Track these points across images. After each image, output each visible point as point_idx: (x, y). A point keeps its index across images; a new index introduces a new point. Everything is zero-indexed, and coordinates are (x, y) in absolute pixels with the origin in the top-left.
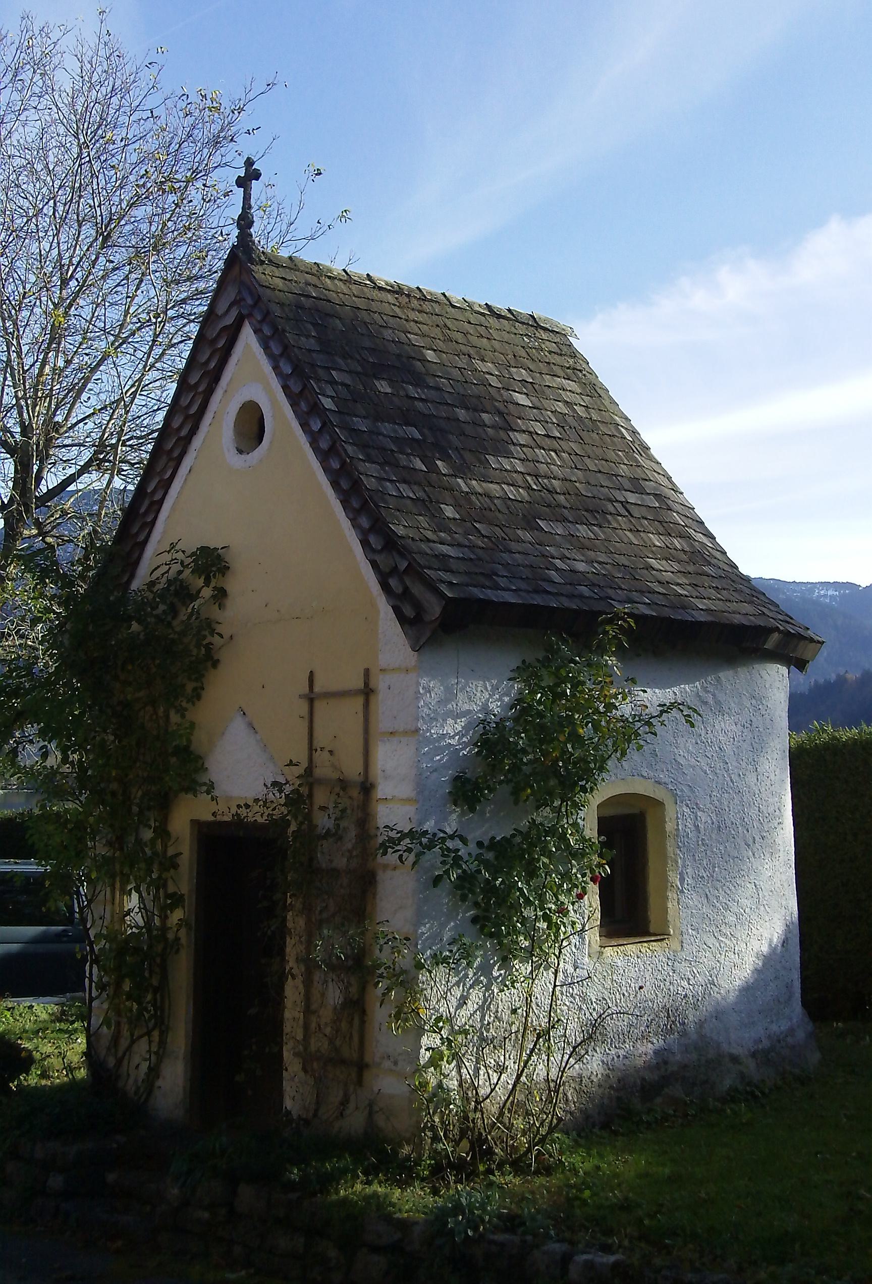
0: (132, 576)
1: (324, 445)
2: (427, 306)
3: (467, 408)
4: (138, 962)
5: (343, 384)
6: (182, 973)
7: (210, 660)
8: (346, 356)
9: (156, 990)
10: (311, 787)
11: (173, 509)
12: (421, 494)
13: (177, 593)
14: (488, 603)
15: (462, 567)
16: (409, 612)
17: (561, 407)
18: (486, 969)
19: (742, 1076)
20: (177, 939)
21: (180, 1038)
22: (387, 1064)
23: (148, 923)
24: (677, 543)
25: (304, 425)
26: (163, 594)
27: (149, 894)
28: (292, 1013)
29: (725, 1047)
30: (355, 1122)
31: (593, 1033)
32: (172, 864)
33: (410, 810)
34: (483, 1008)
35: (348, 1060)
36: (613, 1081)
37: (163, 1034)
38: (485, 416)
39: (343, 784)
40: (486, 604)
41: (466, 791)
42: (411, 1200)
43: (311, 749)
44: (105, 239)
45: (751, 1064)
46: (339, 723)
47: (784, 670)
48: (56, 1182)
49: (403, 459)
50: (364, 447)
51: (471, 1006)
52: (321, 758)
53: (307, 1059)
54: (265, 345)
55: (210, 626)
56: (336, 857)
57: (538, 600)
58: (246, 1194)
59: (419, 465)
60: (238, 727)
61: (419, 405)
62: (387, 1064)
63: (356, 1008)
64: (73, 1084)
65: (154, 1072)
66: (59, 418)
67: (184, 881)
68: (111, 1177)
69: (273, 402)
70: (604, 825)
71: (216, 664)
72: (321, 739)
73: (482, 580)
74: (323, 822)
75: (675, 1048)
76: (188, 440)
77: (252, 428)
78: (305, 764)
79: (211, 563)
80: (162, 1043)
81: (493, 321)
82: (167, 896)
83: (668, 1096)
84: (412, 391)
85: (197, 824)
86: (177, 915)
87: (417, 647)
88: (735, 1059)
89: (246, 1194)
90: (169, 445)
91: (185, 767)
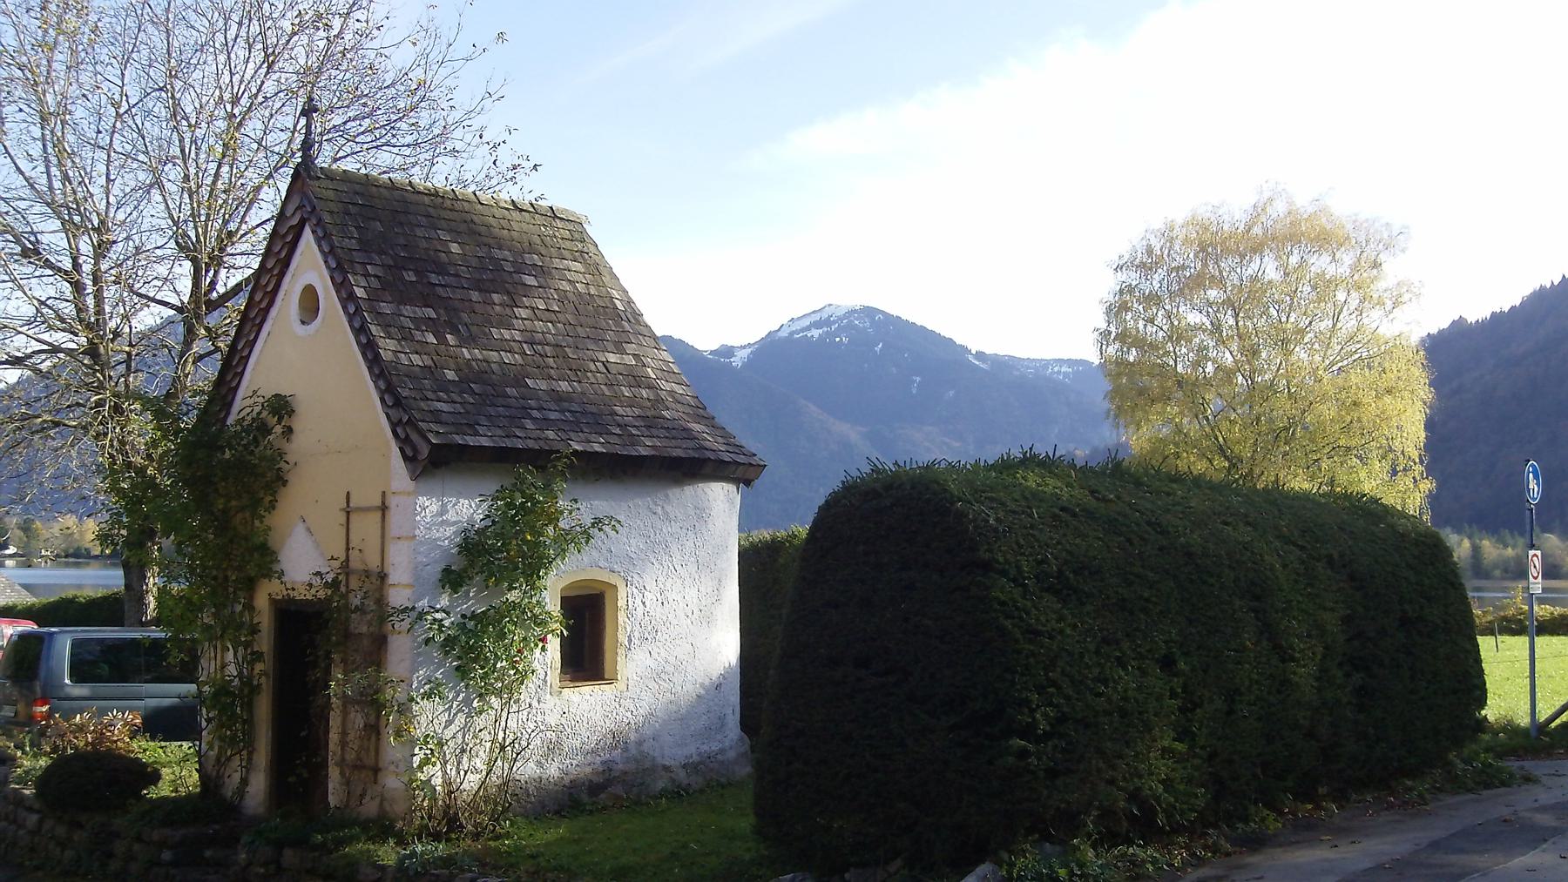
0: (228, 414)
1: (357, 325)
2: (458, 206)
3: (480, 291)
4: (230, 702)
5: (375, 276)
6: (263, 708)
7: (281, 480)
8: (381, 252)
9: (245, 722)
10: (347, 574)
11: (257, 363)
12: (429, 363)
13: (258, 428)
14: (466, 446)
15: (451, 419)
16: (409, 453)
17: (565, 286)
18: (467, 702)
19: (673, 780)
20: (259, 685)
21: (262, 757)
22: (392, 768)
23: (240, 674)
24: (644, 393)
25: (345, 308)
26: (247, 430)
27: (1544, 809)
28: (334, 737)
29: (659, 761)
30: (370, 808)
31: (553, 749)
32: (254, 630)
33: (407, 592)
34: (465, 729)
35: (369, 768)
36: (567, 780)
37: (250, 754)
38: (495, 296)
39: (367, 573)
40: (465, 448)
41: (452, 579)
42: (388, 854)
43: (348, 549)
44: (269, 67)
45: (682, 774)
46: (365, 528)
47: (731, 487)
48: (167, 855)
49: (418, 335)
50: (386, 326)
51: (453, 728)
52: (354, 554)
53: (342, 763)
54: (318, 241)
55: (281, 454)
56: (360, 626)
57: (508, 443)
58: (289, 856)
59: (431, 339)
60: (300, 530)
61: (440, 291)
62: (392, 768)
63: (374, 730)
64: (189, 796)
65: (244, 782)
66: (232, 226)
67: (265, 642)
68: (208, 853)
69: (325, 288)
70: (566, 602)
71: (285, 483)
72: (354, 542)
73: (465, 428)
74: (355, 601)
75: (618, 760)
76: (267, 310)
77: (310, 305)
78: (343, 558)
79: (281, 407)
80: (250, 759)
81: (516, 215)
82: (253, 653)
83: (610, 792)
84: (434, 278)
85: (274, 602)
86: (259, 667)
87: (415, 478)
88: (666, 768)
89: (289, 856)
90: (252, 315)
91: (265, 559)
